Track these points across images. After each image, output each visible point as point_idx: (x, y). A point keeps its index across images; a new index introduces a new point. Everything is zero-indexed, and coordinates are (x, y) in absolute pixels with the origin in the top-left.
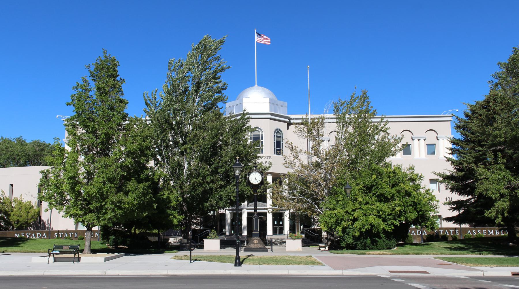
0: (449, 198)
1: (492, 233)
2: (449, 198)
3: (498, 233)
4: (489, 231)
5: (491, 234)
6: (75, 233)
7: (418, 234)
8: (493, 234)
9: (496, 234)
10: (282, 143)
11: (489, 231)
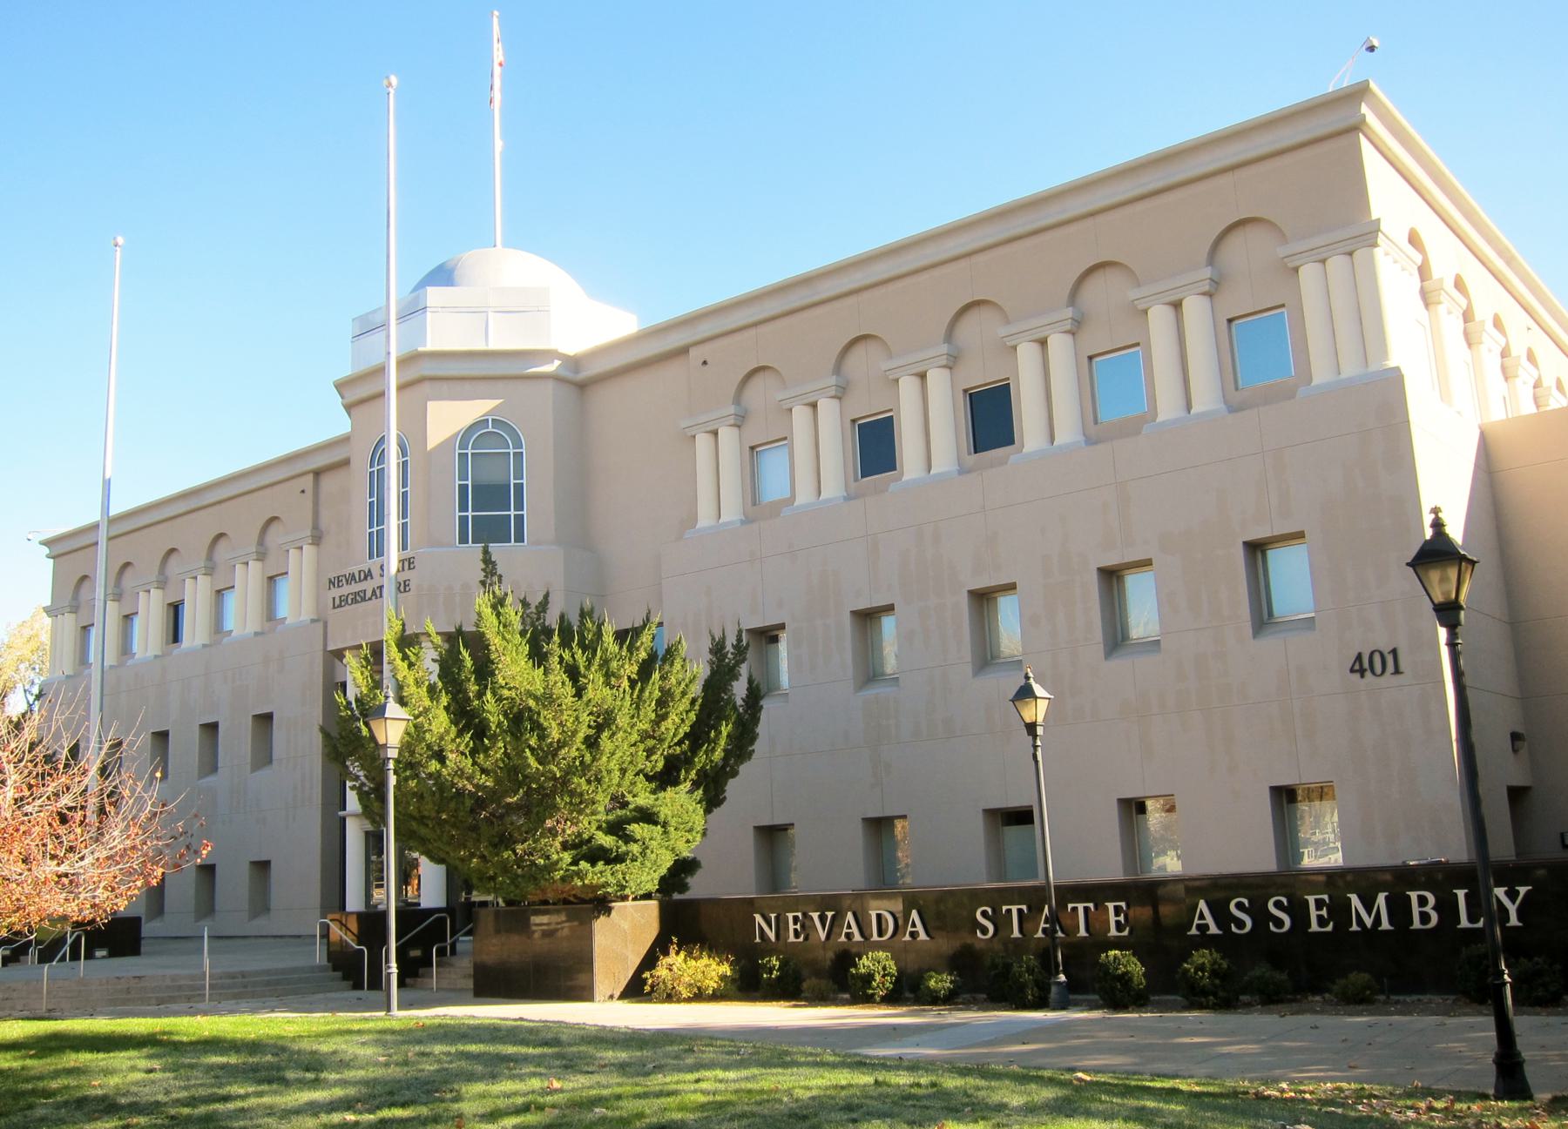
0: (1377, 658)
1: (1378, 920)
2: (1377, 658)
3: (1425, 918)
5: (1369, 922)
6: (790, 916)
7: (875, 937)
8: (1385, 925)
9: (1417, 924)
10: (512, 482)
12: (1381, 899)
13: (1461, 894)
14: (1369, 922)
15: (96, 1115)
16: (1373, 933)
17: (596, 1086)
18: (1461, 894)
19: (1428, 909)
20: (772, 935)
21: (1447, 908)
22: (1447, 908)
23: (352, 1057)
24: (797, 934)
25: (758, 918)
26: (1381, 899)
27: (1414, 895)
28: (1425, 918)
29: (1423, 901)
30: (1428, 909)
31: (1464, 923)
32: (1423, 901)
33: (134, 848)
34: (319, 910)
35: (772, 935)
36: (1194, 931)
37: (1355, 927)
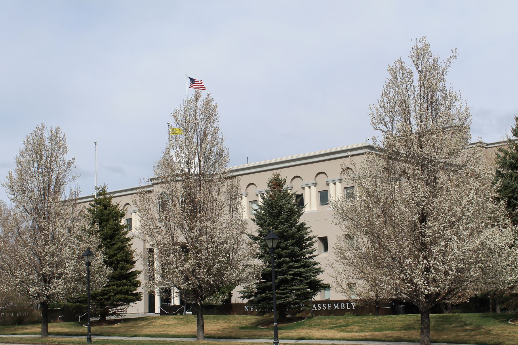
3: (343, 307)
4: (334, 304)
5: (336, 308)
8: (338, 309)
9: (342, 309)
11: (334, 304)
12: (338, 304)
13: (347, 304)
14: (336, 308)
15: (120, 303)
16: (336, 310)
17: (111, 247)
18: (347, 304)
19: (343, 306)
20: (248, 310)
21: (346, 306)
22: (346, 306)
23: (456, 122)
24: (330, 308)
25: (245, 307)
26: (338, 304)
27: (342, 304)
28: (343, 307)
29: (343, 305)
30: (343, 306)
31: (348, 308)
32: (343, 305)
33: (499, 212)
34: (143, 307)
35: (248, 310)
36: (313, 309)
37: (334, 309)
